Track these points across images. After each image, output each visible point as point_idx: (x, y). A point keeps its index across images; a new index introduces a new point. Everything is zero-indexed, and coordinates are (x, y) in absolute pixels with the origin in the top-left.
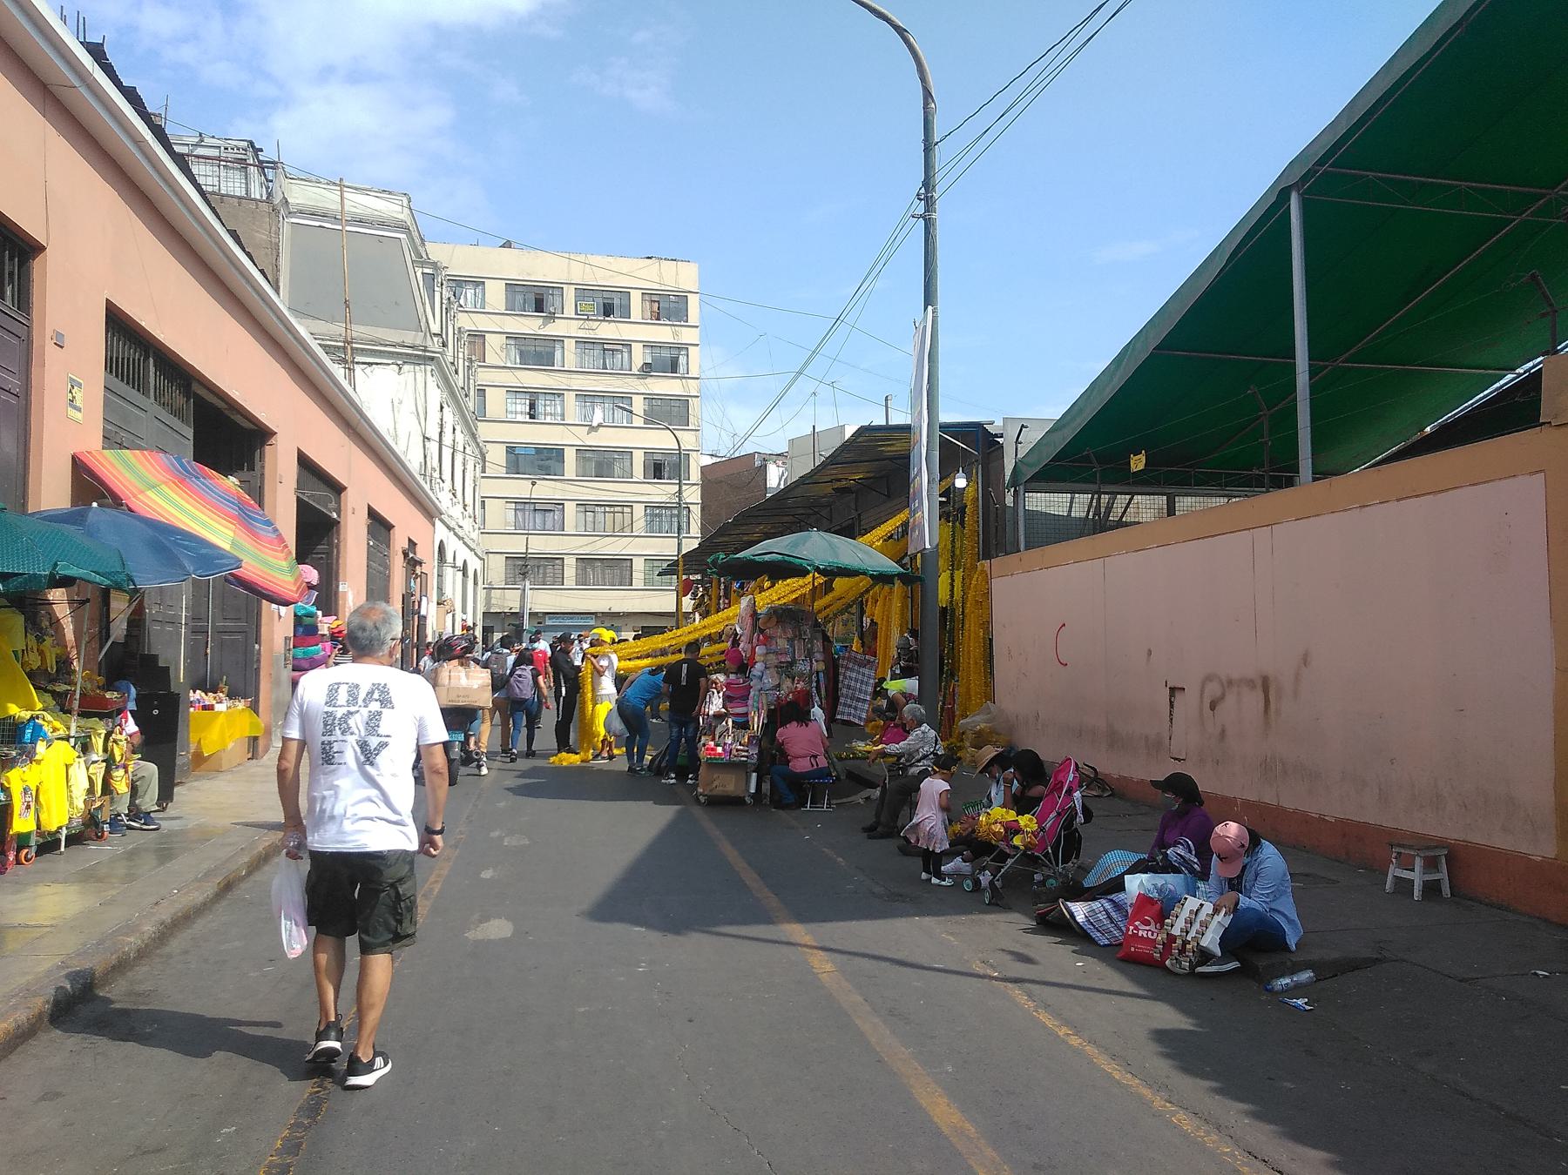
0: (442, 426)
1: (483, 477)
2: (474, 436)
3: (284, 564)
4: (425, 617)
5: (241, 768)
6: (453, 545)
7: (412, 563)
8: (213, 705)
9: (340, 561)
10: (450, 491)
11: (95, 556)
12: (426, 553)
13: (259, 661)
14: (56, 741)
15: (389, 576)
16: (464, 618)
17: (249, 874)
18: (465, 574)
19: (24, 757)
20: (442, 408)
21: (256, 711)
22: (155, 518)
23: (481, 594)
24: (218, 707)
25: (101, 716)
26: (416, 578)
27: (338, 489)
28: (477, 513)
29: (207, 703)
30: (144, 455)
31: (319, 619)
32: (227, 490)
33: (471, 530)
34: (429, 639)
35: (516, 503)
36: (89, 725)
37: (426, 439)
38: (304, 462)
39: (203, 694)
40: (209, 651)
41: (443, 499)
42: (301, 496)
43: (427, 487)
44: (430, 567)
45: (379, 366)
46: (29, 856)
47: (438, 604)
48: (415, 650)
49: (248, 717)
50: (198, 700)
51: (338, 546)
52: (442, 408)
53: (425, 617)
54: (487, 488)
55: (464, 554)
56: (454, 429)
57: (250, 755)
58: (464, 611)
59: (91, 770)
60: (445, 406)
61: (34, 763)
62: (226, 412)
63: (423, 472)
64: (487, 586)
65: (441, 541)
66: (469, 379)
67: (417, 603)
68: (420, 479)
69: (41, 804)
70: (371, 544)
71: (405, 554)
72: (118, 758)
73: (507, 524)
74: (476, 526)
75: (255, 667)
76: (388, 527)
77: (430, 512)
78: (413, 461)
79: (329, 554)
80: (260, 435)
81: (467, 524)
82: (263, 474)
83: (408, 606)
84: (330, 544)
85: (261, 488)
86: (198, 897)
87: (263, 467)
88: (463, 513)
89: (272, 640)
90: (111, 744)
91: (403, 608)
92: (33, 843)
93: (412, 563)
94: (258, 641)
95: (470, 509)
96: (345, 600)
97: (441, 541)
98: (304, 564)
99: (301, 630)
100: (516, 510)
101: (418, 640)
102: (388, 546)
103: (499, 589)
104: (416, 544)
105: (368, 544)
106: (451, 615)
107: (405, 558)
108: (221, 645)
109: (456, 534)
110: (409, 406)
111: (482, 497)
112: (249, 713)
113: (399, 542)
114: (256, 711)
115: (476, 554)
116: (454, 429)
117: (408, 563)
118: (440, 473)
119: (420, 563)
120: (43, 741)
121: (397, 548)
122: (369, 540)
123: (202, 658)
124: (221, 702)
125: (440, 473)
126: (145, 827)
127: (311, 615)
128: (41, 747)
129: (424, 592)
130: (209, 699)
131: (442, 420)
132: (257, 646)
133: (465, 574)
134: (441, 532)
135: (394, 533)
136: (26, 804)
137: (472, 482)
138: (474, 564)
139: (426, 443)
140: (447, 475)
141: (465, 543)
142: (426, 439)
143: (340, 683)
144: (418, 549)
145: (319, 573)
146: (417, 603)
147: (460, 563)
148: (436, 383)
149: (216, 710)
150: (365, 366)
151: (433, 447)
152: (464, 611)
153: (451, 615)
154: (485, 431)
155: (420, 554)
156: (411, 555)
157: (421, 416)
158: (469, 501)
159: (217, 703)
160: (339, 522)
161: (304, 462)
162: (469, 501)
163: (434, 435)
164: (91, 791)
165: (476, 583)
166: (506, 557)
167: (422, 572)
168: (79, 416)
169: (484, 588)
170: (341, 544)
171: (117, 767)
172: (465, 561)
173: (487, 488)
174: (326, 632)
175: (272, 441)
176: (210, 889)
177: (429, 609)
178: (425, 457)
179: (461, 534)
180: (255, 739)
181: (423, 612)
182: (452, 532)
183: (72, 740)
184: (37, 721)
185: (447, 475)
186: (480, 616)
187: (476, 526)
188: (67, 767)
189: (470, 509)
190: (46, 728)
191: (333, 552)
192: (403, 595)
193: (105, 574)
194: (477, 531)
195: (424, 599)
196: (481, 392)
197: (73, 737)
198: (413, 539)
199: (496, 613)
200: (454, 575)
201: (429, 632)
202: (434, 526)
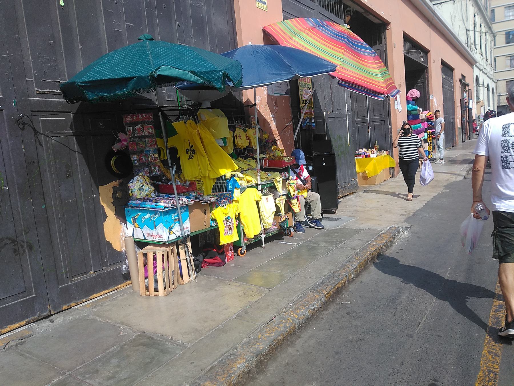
0: (475, 24)
1: (495, 48)
2: (490, 28)
3: (377, 71)
4: (471, 109)
5: (385, 182)
6: (482, 78)
7: (464, 86)
8: (370, 155)
9: (430, 85)
10: (480, 53)
11: (145, 48)
12: (470, 81)
13: (391, 133)
14: (247, 188)
15: (454, 92)
16: (489, 109)
17: (358, 275)
18: (488, 90)
19: (224, 200)
20: (475, 16)
21: (392, 156)
22: (290, 47)
23: (496, 98)
24: (372, 156)
25: (281, 171)
26: (466, 92)
27: (426, 52)
28: (492, 63)
29: (368, 154)
30: (297, 21)
31: (420, 112)
32: (341, 31)
33: (490, 70)
34: (474, 118)
35: (511, 56)
36: (273, 177)
37: (468, 30)
38: (407, 38)
39: (366, 150)
40: (369, 131)
41: (477, 56)
42: (406, 55)
43: (469, 49)
44: (473, 86)
45: (445, 3)
46: (243, 252)
47: (477, 103)
48: (468, 123)
49: (388, 159)
50: (364, 153)
51: (428, 79)
52: (475, 16)
53: (471, 109)
54: (497, 53)
55: (487, 81)
56: (481, 26)
57: (391, 176)
58: (489, 106)
59: (277, 201)
60: (476, 15)
61: (233, 202)
62: (365, 15)
63: (467, 42)
64: (498, 95)
65: (477, 76)
66: (487, 3)
67: (467, 103)
68: (466, 46)
69: (243, 224)
70: (444, 77)
71: (461, 81)
72: (292, 194)
73: (506, 67)
74: (492, 69)
75: (390, 136)
76: (452, 69)
77: (471, 62)
78: (462, 39)
79: (424, 83)
80: (384, 25)
81: (488, 68)
82: (386, 45)
83: (463, 104)
84: (424, 78)
85: (386, 52)
86: (304, 313)
87: (386, 41)
88: (486, 63)
89: (397, 123)
90: (287, 186)
91: (461, 105)
92: (243, 245)
93: (464, 85)
94: (390, 124)
95: (489, 61)
96: (433, 102)
97: (477, 76)
98: (414, 89)
99: (411, 117)
100: (511, 60)
101: (469, 119)
102: (452, 78)
103: (504, 95)
104: (465, 77)
105: (442, 77)
106: (483, 107)
107: (460, 83)
108: (374, 127)
109: (483, 72)
110: (458, 17)
111: (495, 57)
112: (388, 157)
113: (457, 76)
114: (392, 156)
115: (493, 81)
116: (481, 26)
117: (462, 85)
118: (475, 46)
119: (468, 85)
120: (238, 189)
121: (456, 79)
122: (442, 75)
123: (367, 134)
124: (373, 153)
125: (475, 46)
126: (316, 227)
127: (415, 110)
128: (237, 193)
129: (470, 98)
130: (369, 152)
131: (475, 21)
132: (390, 126)
133: (488, 90)
134: (476, 72)
135: (455, 72)
136: (228, 227)
137: (490, 49)
138: (492, 85)
139: (468, 33)
140: (478, 47)
141: (488, 76)
142: (468, 30)
143: (510, 124)
144: (466, 79)
145: (420, 92)
146: (467, 103)
147: (486, 84)
148: (471, 4)
149: (371, 157)
150: (439, 5)
151: (471, 33)
152: (489, 106)
153: (483, 107)
154: (496, 28)
155: (467, 81)
156: (463, 82)
157: (465, 20)
158: (489, 57)
159: (372, 154)
160: (428, 67)
161: (407, 38)
162: (489, 57)
163: (471, 28)
164: (277, 213)
165: (493, 93)
166: (507, 81)
167: (469, 89)
168: (265, 7)
169: (497, 96)
170: (429, 77)
171: (293, 198)
172: (488, 84)
173: (497, 53)
174: (424, 118)
175: (389, 27)
176: (321, 297)
177: (473, 104)
178: (467, 39)
179: (486, 72)
180: (393, 168)
181: (470, 107)
182: (482, 72)
183: (260, 188)
184: (235, 178)
185: (478, 47)
186: (496, 107)
187: (492, 69)
188: (257, 202)
189: (489, 61)
190: (239, 182)
191: (426, 82)
192: (461, 100)
193: (202, 73)
194: (493, 71)
195: (470, 101)
196: (493, 11)
197: (260, 185)
198: (463, 74)
199: (503, 106)
200: (484, 90)
201: (474, 115)
202: (473, 68)
